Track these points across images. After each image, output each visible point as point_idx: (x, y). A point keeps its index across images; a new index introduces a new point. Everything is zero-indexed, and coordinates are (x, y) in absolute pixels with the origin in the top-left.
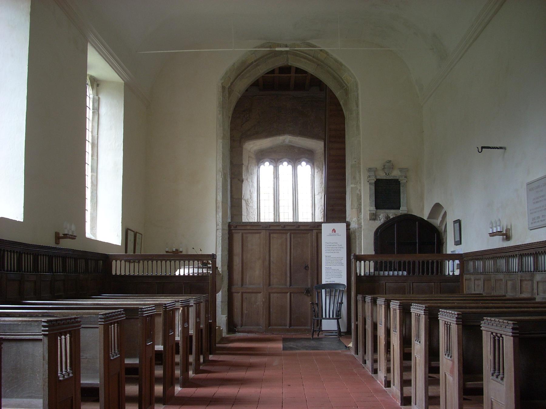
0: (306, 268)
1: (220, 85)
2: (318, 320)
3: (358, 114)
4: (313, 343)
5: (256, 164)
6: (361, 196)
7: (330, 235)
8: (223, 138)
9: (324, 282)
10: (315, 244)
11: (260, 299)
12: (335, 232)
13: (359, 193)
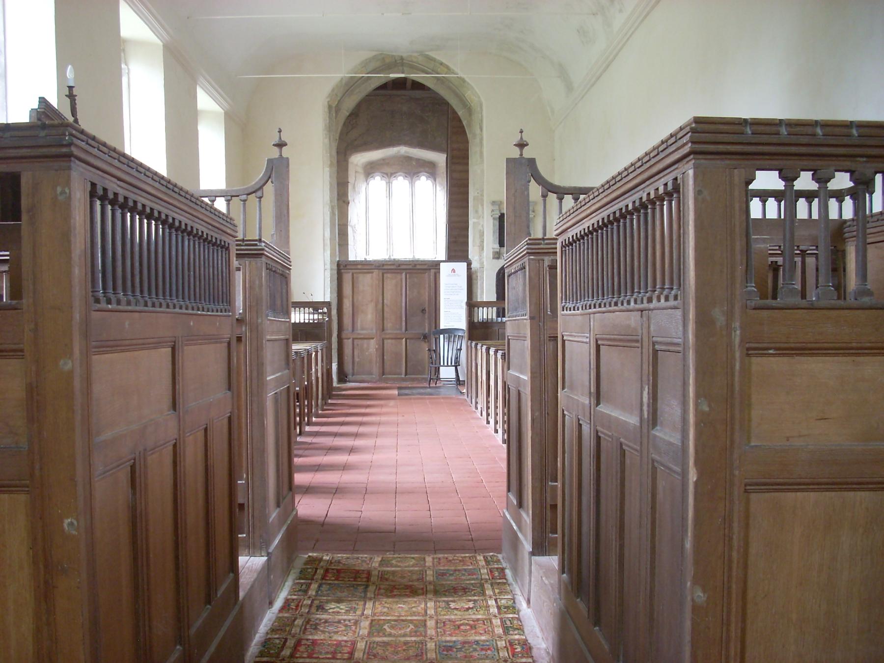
0: (423, 311)
1: (326, 103)
2: (436, 367)
3: (481, 139)
4: (429, 390)
5: (364, 179)
6: (483, 232)
7: (449, 275)
8: (331, 166)
9: (442, 327)
10: (433, 285)
11: (372, 346)
12: (454, 272)
13: (482, 229)
